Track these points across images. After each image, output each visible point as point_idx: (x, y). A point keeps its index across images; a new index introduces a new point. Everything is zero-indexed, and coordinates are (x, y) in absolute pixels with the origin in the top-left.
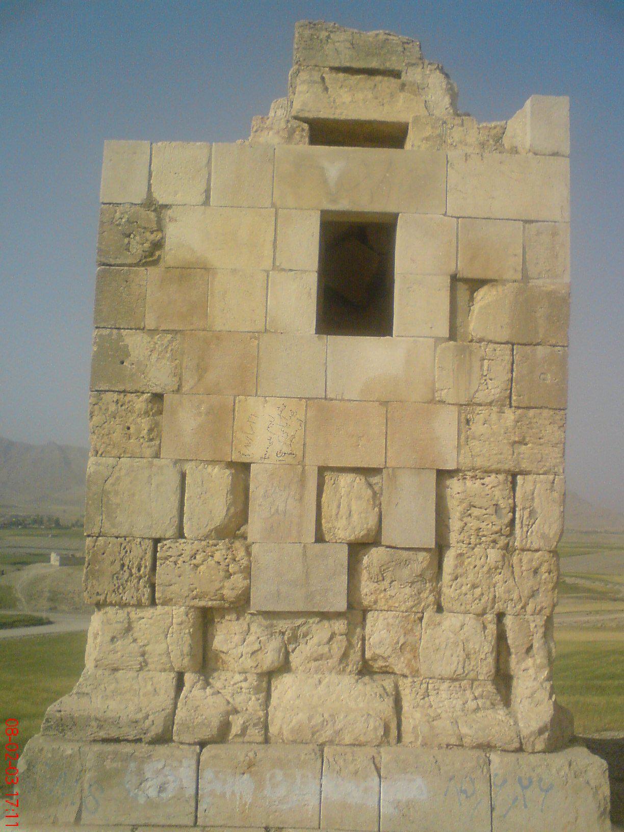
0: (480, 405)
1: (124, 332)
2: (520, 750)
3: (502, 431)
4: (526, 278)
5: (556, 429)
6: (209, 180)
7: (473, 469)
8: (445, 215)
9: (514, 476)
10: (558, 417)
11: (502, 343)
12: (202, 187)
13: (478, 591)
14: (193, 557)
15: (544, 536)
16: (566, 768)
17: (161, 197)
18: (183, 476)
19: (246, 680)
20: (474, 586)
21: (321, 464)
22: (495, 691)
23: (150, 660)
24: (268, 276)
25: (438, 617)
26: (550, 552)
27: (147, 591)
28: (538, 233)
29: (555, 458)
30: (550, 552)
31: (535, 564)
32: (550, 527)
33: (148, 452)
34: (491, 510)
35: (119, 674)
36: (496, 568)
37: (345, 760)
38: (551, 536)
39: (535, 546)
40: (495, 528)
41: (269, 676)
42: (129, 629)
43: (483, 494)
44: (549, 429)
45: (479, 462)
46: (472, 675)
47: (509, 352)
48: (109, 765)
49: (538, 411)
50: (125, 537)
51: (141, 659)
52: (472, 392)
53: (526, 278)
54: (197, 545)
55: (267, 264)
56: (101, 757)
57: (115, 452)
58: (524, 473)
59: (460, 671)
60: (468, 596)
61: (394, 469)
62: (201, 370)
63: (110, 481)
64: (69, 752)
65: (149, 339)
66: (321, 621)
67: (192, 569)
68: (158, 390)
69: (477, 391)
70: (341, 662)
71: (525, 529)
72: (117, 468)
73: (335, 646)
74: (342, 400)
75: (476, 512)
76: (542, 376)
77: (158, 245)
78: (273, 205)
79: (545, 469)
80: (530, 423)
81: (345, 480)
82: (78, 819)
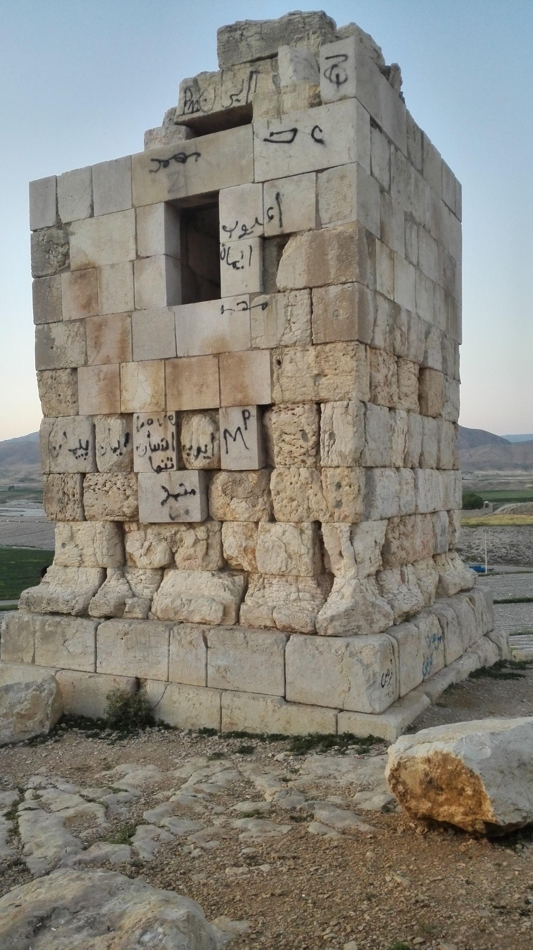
0: (286, 346)
1: (52, 325)
2: (314, 633)
3: (305, 367)
4: (319, 224)
5: (348, 359)
6: (92, 196)
7: (283, 402)
8: (253, 182)
9: (318, 404)
10: (351, 348)
11: (301, 289)
12: (88, 203)
13: (295, 503)
14: (104, 485)
15: (341, 454)
16: (343, 649)
17: (64, 219)
18: (94, 426)
19: (145, 573)
20: (292, 500)
21: (177, 409)
22: (314, 586)
23: (85, 560)
24: (133, 265)
25: (268, 526)
26: (348, 467)
27: (79, 510)
28: (329, 181)
29: (349, 386)
30: (348, 467)
31: (337, 480)
32: (346, 446)
33: (72, 412)
34: (299, 435)
35: (68, 570)
36: (307, 483)
37: (185, 632)
38: (347, 454)
39: (335, 463)
40: (303, 451)
41: (163, 569)
42: (72, 537)
43: (292, 422)
44: (343, 358)
45: (288, 395)
46: (294, 572)
47: (307, 296)
48: (47, 628)
49: (333, 345)
50: (64, 473)
51: (79, 558)
52: (279, 336)
53: (319, 224)
54: (105, 477)
55: (133, 256)
56: (43, 624)
57: (54, 414)
58: (326, 401)
59: (284, 569)
60: (288, 508)
61: (226, 407)
62: (97, 345)
63: (52, 434)
64: (27, 619)
65: (66, 328)
66: (188, 529)
67: (104, 494)
68: (73, 365)
69: (283, 335)
70: (203, 560)
71: (326, 449)
72: (55, 425)
73: (198, 549)
74: (188, 357)
75: (287, 438)
76: (336, 313)
77: (66, 255)
78: (133, 206)
79: (340, 395)
80: (327, 357)
81: (196, 420)
82: (33, 661)
